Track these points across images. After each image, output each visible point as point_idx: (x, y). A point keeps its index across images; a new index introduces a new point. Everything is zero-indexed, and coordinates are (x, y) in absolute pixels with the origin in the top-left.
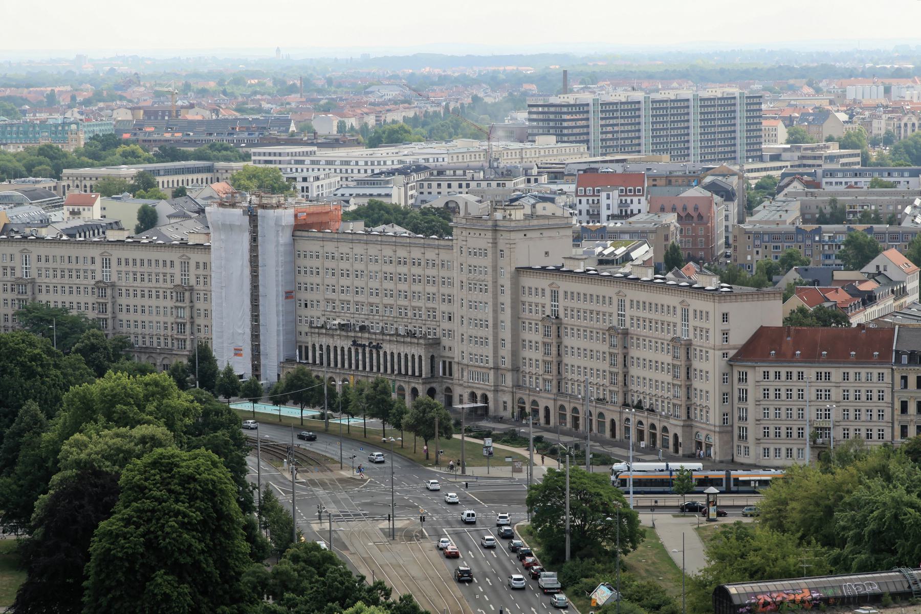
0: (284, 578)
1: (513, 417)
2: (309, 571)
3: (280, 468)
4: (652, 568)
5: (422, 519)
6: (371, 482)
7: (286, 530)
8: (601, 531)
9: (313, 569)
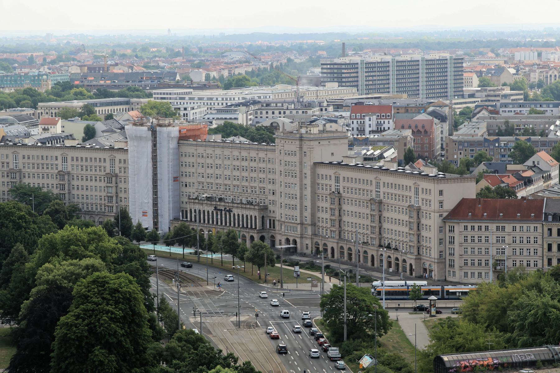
0: (173, 351)
1: (312, 253)
2: (188, 347)
3: (170, 284)
4: (396, 345)
5: (257, 315)
6: (225, 293)
7: (174, 322)
8: (366, 322)
9: (190, 346)
